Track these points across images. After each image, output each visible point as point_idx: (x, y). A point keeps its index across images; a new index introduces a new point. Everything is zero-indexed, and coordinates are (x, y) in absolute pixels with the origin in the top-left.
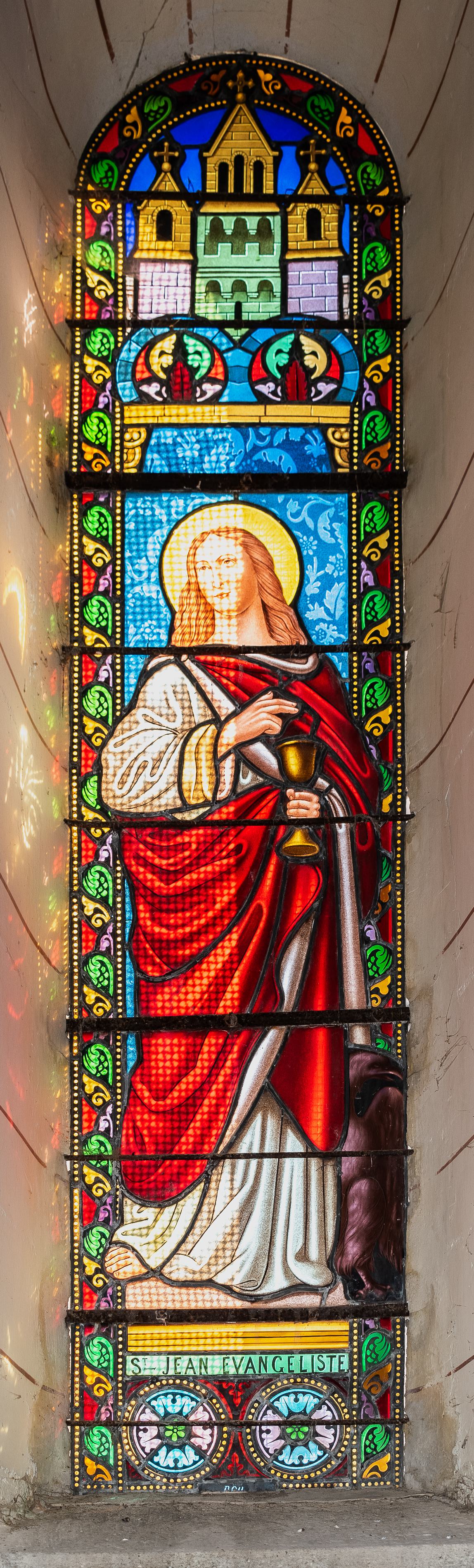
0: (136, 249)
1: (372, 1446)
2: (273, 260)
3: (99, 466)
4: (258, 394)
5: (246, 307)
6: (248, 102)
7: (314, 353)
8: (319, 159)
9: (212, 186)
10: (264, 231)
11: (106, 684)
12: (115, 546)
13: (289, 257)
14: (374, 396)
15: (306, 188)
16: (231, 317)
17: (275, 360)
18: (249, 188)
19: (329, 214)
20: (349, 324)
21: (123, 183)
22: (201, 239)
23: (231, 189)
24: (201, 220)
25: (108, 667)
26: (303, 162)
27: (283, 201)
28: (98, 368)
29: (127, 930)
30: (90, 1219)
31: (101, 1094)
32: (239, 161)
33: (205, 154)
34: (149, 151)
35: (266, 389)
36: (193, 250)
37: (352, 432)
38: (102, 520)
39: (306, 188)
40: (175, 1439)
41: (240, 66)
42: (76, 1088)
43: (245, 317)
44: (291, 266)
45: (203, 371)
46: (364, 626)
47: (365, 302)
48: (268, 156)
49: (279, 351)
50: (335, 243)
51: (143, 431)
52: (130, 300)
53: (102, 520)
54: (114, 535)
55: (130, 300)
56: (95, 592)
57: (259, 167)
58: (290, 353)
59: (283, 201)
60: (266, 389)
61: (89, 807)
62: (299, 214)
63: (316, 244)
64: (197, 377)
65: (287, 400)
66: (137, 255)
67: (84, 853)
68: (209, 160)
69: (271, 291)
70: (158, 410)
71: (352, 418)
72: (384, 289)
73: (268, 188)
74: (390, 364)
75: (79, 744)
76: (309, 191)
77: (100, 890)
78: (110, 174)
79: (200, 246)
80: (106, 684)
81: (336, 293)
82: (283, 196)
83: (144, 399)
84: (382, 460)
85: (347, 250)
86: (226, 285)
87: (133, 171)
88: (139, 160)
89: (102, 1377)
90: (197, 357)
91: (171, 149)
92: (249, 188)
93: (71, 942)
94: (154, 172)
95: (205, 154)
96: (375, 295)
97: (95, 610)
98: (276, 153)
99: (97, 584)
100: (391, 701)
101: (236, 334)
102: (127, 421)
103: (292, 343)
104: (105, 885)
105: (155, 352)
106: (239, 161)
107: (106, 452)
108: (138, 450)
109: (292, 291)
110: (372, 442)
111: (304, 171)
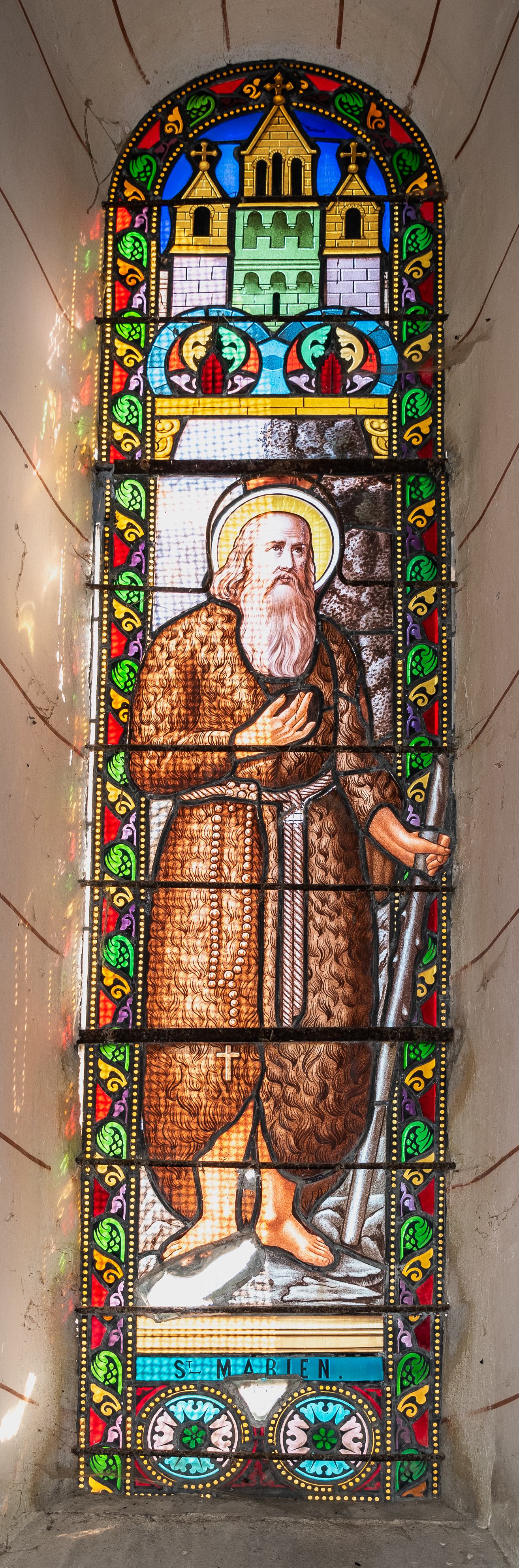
0: (171, 243)
1: (414, 1146)
2: (312, 253)
3: (132, 362)
4: (172, 385)
5: (283, 299)
6: (287, 106)
7: (350, 346)
8: (359, 161)
9: (250, 190)
10: (303, 221)
11: (119, 1215)
12: (136, 978)
13: (326, 252)
14: (413, 292)
15: (345, 189)
16: (269, 311)
17: (311, 351)
18: (287, 189)
19: (369, 212)
20: (391, 317)
21: (158, 187)
22: (239, 231)
23: (269, 191)
24: (239, 214)
25: (142, 295)
26: (344, 164)
27: (324, 202)
28: (129, 352)
29: (151, 865)
30: (101, 1208)
31: (118, 1080)
32: (277, 159)
33: (243, 153)
34: (185, 152)
35: (301, 380)
36: (231, 243)
37: (391, 422)
38: (132, 408)
39: (345, 189)
40: (193, 1445)
41: (280, 70)
42: (86, 1265)
43: (283, 312)
44: (331, 263)
45: (236, 365)
46: (404, 339)
47: (409, 617)
48: (306, 154)
49: (196, 344)
50: (375, 243)
51: (176, 423)
52: (163, 293)
53: (132, 408)
54: (136, 965)
55: (163, 293)
56: (125, 391)
57: (297, 165)
58: (327, 345)
59: (324, 202)
60: (301, 380)
61: (124, 259)
62: (337, 213)
63: (354, 242)
64: (349, 370)
65: (323, 391)
66: (174, 250)
67: (102, 1014)
68: (246, 158)
69: (311, 283)
70: (191, 401)
71: (390, 409)
72: (424, 270)
73: (307, 190)
74: (435, 976)
75: (98, 994)
76: (348, 193)
77: (123, 868)
78: (148, 168)
79: (238, 240)
80: (119, 1215)
81: (378, 289)
82: (324, 197)
83: (178, 392)
84: (427, 695)
85: (387, 250)
86: (265, 278)
87: (170, 169)
88: (176, 159)
89: (136, 269)
90: (348, 350)
91: (209, 148)
92: (287, 189)
93: (106, 251)
94: (189, 171)
95: (243, 153)
96: (415, 276)
97: (129, 245)
98: (314, 151)
99: (128, 383)
100: (432, 246)
101: (273, 326)
102: (158, 412)
103: (328, 335)
104: (135, 414)
105: (191, 340)
106: (277, 159)
107: (136, 432)
108: (170, 439)
109: (331, 286)
110: (413, 418)
111: (345, 173)
